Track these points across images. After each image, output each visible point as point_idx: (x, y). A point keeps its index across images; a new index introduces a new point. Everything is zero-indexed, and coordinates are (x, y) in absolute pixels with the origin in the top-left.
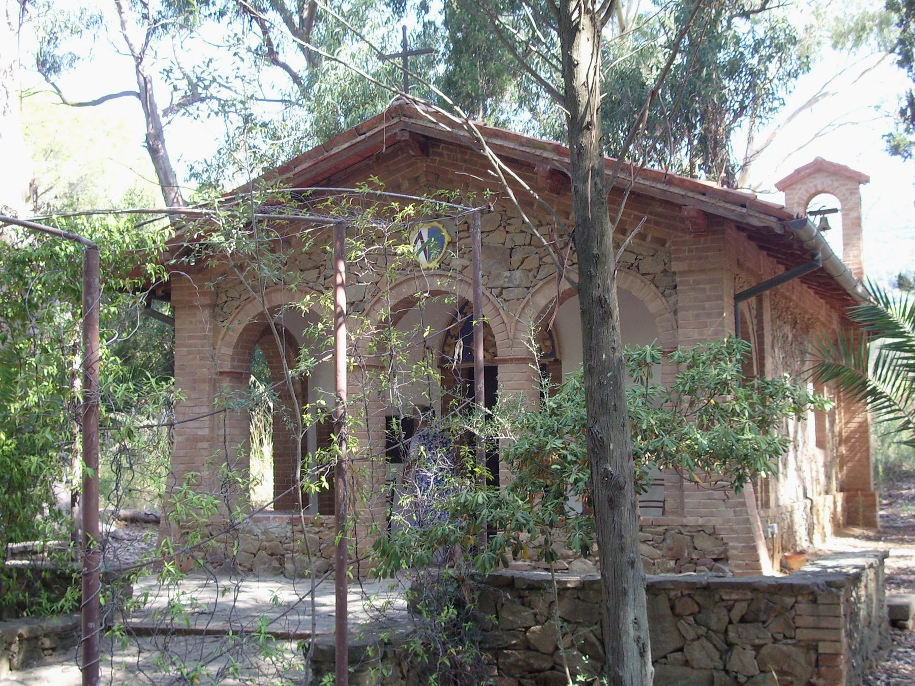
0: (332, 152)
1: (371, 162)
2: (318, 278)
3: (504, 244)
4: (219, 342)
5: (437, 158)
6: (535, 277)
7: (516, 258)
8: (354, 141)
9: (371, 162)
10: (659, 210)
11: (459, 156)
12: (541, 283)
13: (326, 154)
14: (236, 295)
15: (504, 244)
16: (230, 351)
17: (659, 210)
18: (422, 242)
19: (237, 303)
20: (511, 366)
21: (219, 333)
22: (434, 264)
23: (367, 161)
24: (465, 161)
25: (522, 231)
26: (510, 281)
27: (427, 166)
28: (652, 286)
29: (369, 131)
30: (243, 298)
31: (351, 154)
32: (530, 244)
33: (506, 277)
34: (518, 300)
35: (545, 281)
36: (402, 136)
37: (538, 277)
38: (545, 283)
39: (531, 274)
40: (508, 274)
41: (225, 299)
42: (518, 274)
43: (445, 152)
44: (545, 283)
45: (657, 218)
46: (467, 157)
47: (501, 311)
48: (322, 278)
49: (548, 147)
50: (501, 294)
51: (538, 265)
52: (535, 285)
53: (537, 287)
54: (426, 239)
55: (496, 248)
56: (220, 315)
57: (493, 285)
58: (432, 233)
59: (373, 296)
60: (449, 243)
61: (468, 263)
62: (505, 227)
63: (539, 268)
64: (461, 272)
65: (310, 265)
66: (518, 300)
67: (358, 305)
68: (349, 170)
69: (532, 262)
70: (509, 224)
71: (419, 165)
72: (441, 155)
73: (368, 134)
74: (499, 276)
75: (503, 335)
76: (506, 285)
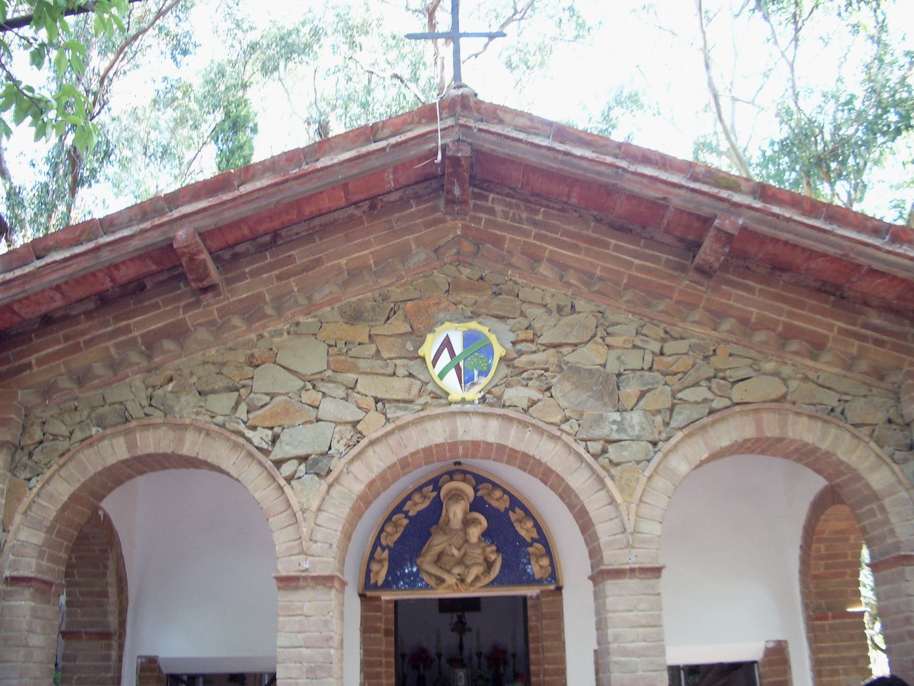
0: (319, 165)
1: (358, 212)
2: (235, 408)
3: (604, 366)
4: (18, 518)
5: (484, 216)
6: (667, 424)
7: (630, 390)
8: (364, 150)
9: (358, 212)
10: (877, 321)
11: (524, 215)
12: (680, 435)
13: (305, 167)
14: (64, 430)
15: (604, 366)
16: (36, 538)
17: (877, 321)
18: (452, 353)
19: (63, 445)
20: (631, 584)
21: (19, 500)
22: (473, 394)
23: (351, 210)
24: (535, 224)
25: (635, 347)
26: (621, 428)
27: (465, 228)
28: (872, 444)
29: (393, 135)
30: (78, 435)
31: (355, 171)
32: (650, 369)
33: (614, 422)
34: (638, 462)
35: (686, 431)
36: (458, 150)
37: (673, 424)
38: (687, 436)
39: (659, 419)
40: (616, 416)
41: (38, 436)
42: (635, 418)
43: (498, 208)
44: (687, 436)
45: (876, 335)
46: (539, 217)
47: (608, 481)
48: (243, 408)
49: (744, 186)
50: (604, 451)
51: (669, 405)
52: (668, 439)
53: (673, 441)
54: (458, 349)
55: (590, 372)
56: (25, 466)
57: (590, 436)
58: (470, 339)
59: (349, 446)
60: (501, 359)
61: (536, 395)
62: (603, 338)
63: (672, 410)
64: (525, 411)
65: (221, 383)
66: (638, 462)
67: (316, 462)
68: (317, 222)
69: (660, 398)
70: (608, 334)
71: (449, 224)
72: (491, 211)
73: (393, 141)
74: (600, 419)
75: (614, 525)
76: (615, 436)
